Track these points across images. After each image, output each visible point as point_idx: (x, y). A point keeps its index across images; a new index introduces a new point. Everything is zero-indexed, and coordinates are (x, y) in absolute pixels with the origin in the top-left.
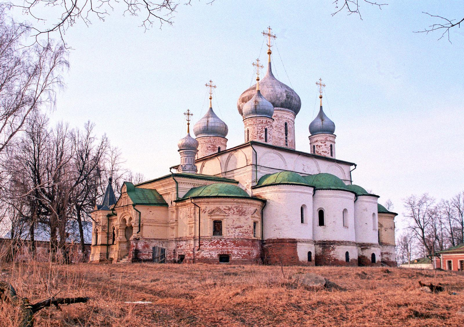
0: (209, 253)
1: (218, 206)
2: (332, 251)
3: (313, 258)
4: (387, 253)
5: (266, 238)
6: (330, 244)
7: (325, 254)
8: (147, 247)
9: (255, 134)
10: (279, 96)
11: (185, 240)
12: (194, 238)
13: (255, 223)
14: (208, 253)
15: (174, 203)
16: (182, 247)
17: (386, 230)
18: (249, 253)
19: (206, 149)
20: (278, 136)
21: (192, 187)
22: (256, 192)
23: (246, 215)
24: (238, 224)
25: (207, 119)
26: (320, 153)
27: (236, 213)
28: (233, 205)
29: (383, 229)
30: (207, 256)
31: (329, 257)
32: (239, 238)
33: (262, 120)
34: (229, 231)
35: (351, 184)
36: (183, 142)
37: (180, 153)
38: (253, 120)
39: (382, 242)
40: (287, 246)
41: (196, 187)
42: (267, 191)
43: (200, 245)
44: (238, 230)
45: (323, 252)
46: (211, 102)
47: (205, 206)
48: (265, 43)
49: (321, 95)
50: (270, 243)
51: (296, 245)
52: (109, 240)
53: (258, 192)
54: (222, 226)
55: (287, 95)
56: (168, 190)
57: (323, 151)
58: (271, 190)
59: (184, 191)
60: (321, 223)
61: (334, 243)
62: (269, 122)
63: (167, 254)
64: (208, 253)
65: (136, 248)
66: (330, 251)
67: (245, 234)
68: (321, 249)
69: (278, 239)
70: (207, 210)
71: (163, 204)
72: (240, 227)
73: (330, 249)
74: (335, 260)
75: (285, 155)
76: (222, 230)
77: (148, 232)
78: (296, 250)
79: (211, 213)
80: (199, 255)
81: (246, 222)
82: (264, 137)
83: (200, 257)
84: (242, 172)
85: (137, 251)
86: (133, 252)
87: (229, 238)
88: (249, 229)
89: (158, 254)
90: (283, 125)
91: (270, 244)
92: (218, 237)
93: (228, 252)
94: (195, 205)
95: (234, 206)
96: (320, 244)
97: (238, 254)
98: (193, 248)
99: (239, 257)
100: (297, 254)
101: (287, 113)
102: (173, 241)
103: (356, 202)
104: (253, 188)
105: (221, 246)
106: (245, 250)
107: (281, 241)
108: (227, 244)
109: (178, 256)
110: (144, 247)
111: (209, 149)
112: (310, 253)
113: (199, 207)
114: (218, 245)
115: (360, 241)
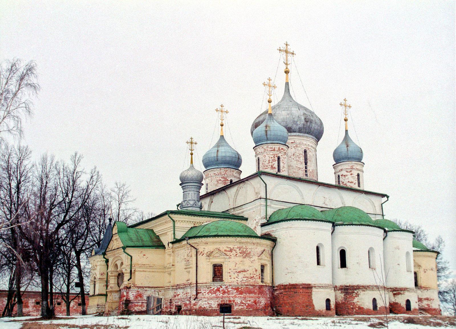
0: (208, 303)
2: (356, 298)
3: (333, 306)
4: (427, 299)
5: (277, 283)
6: (353, 289)
7: (348, 301)
10: (296, 120)
11: (182, 288)
13: (263, 267)
14: (206, 303)
15: (170, 245)
17: (425, 272)
18: (255, 302)
19: (216, 183)
20: (297, 166)
21: (192, 226)
22: (267, 229)
23: (251, 256)
24: (242, 268)
25: (216, 149)
26: (346, 184)
27: (239, 254)
28: (234, 246)
29: (422, 270)
31: (353, 305)
32: (243, 284)
33: (273, 147)
34: (230, 276)
35: (383, 218)
37: (182, 187)
39: (421, 286)
40: (300, 293)
41: (197, 225)
44: (241, 275)
45: (345, 299)
46: (222, 129)
47: (203, 247)
48: (282, 60)
49: (346, 118)
50: (280, 289)
51: (311, 291)
53: (268, 230)
54: (222, 271)
55: (305, 119)
57: (349, 182)
60: (343, 264)
61: (358, 287)
62: (282, 149)
63: (163, 305)
64: (206, 303)
65: (126, 299)
66: (354, 298)
67: (250, 279)
68: (343, 295)
69: (290, 285)
70: (205, 252)
71: (159, 245)
72: (244, 271)
73: (354, 295)
74: (360, 308)
75: (301, 186)
76: (222, 275)
77: (140, 279)
78: (312, 297)
79: (210, 255)
81: (251, 265)
82: (277, 167)
83: (197, 307)
85: (128, 302)
86: (123, 303)
87: (230, 284)
88: (255, 273)
89: (153, 304)
90: (301, 153)
91: (281, 291)
92: (217, 284)
93: (230, 301)
95: (236, 247)
96: (341, 289)
98: (189, 297)
99: (243, 307)
100: (312, 302)
101: (307, 139)
102: (169, 289)
103: (333, 233)
104: (263, 225)
105: (221, 294)
106: (250, 299)
107: (294, 287)
108: (228, 291)
111: (220, 182)
112: (328, 301)
113: (196, 249)
114: (218, 293)
115: (392, 284)
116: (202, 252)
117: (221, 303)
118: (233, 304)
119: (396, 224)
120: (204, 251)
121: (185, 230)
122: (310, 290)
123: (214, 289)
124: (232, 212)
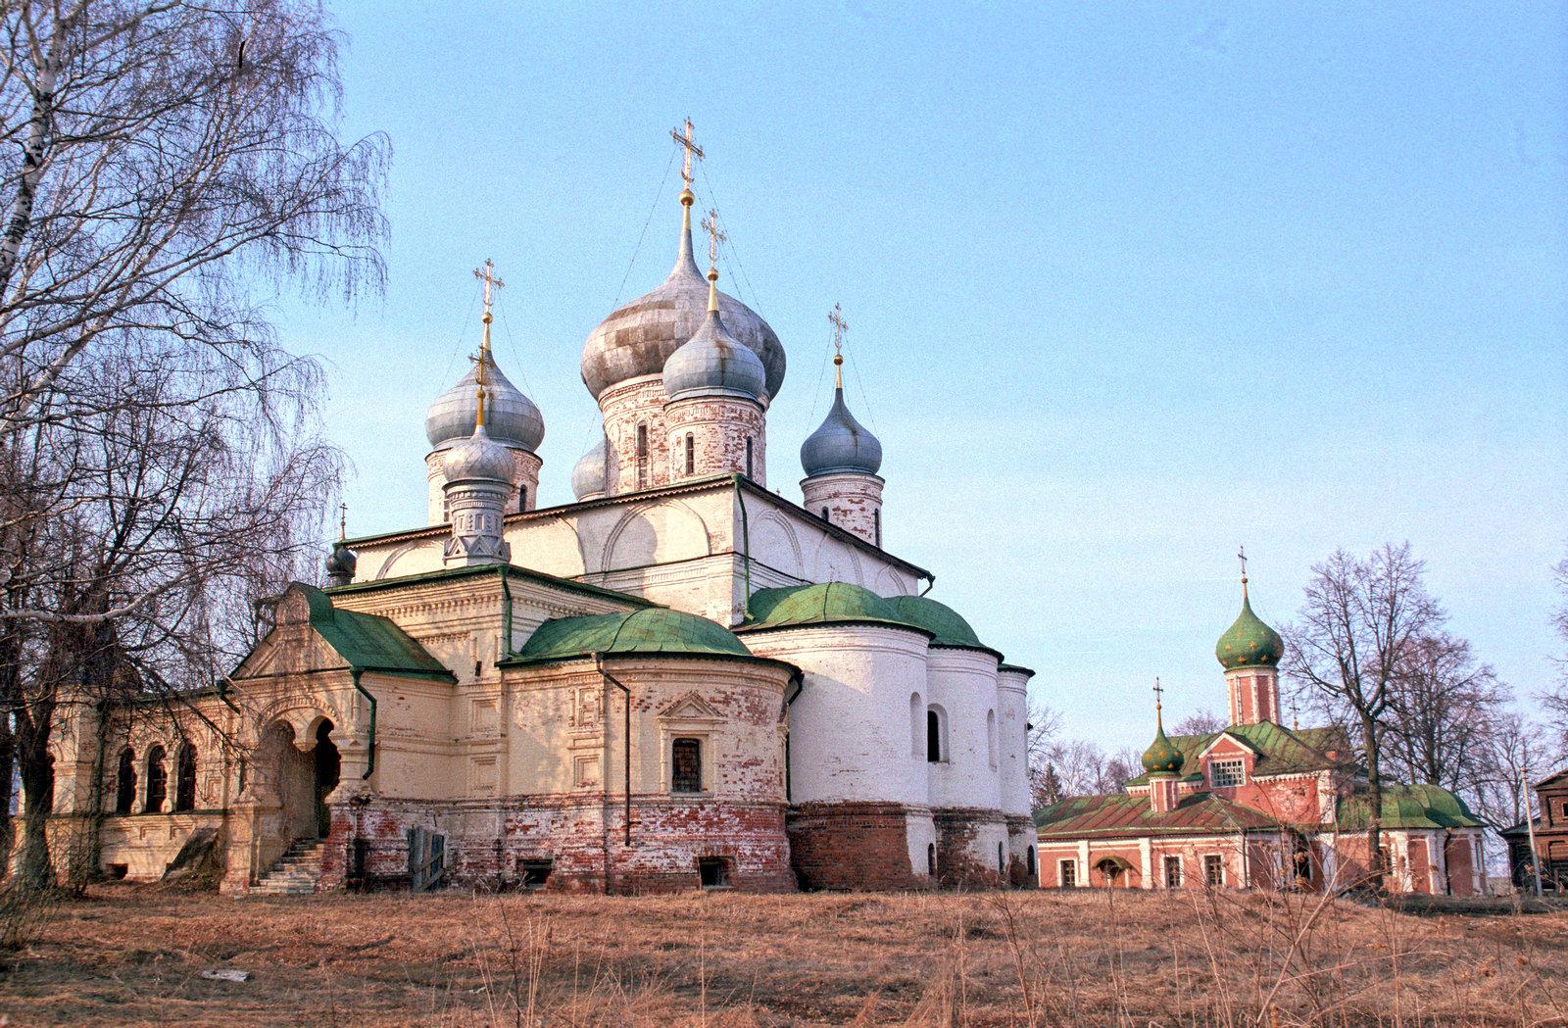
1: (694, 687)
8: (392, 829)
9: (718, 452)
12: (607, 802)
14: (661, 853)
16: (532, 832)
28: (736, 686)
30: (658, 865)
34: (725, 776)
36: (472, 459)
38: (714, 406)
42: (801, 643)
43: (629, 825)
44: (750, 774)
50: (818, 816)
52: (104, 798)
56: (455, 623)
58: (819, 642)
59: (522, 628)
64: (661, 853)
65: (357, 836)
66: (966, 842)
69: (847, 804)
70: (655, 702)
72: (756, 762)
77: (396, 775)
79: (670, 713)
80: (625, 861)
84: (682, 576)
86: (349, 850)
87: (728, 799)
93: (726, 849)
94: (607, 676)
95: (739, 690)
97: (754, 855)
99: (755, 867)
102: (487, 808)
105: (702, 830)
107: (859, 812)
109: (513, 863)
110: (381, 831)
113: (625, 689)
114: (692, 825)
116: (642, 701)
117: (704, 854)
118: (733, 858)
119: (561, 637)
120: (649, 697)
121: (527, 629)
122: (898, 822)
123: (681, 812)
124: (597, 582)
